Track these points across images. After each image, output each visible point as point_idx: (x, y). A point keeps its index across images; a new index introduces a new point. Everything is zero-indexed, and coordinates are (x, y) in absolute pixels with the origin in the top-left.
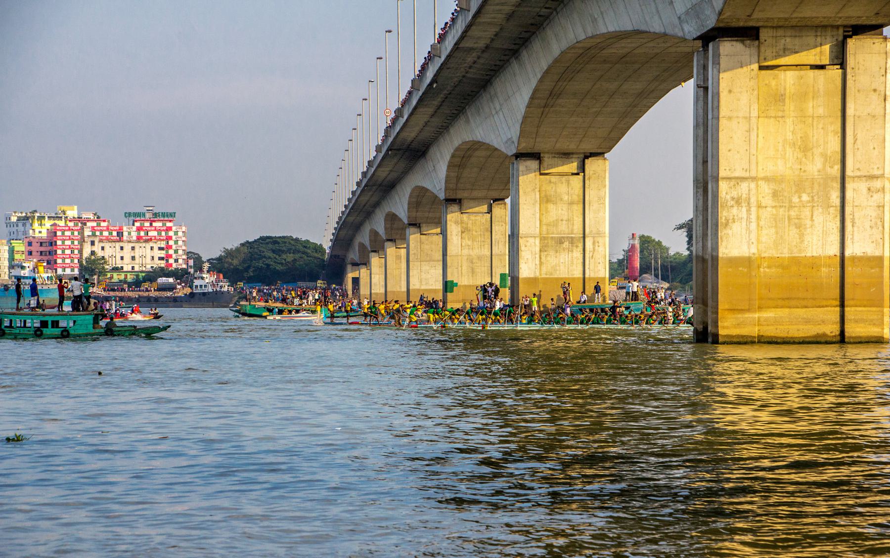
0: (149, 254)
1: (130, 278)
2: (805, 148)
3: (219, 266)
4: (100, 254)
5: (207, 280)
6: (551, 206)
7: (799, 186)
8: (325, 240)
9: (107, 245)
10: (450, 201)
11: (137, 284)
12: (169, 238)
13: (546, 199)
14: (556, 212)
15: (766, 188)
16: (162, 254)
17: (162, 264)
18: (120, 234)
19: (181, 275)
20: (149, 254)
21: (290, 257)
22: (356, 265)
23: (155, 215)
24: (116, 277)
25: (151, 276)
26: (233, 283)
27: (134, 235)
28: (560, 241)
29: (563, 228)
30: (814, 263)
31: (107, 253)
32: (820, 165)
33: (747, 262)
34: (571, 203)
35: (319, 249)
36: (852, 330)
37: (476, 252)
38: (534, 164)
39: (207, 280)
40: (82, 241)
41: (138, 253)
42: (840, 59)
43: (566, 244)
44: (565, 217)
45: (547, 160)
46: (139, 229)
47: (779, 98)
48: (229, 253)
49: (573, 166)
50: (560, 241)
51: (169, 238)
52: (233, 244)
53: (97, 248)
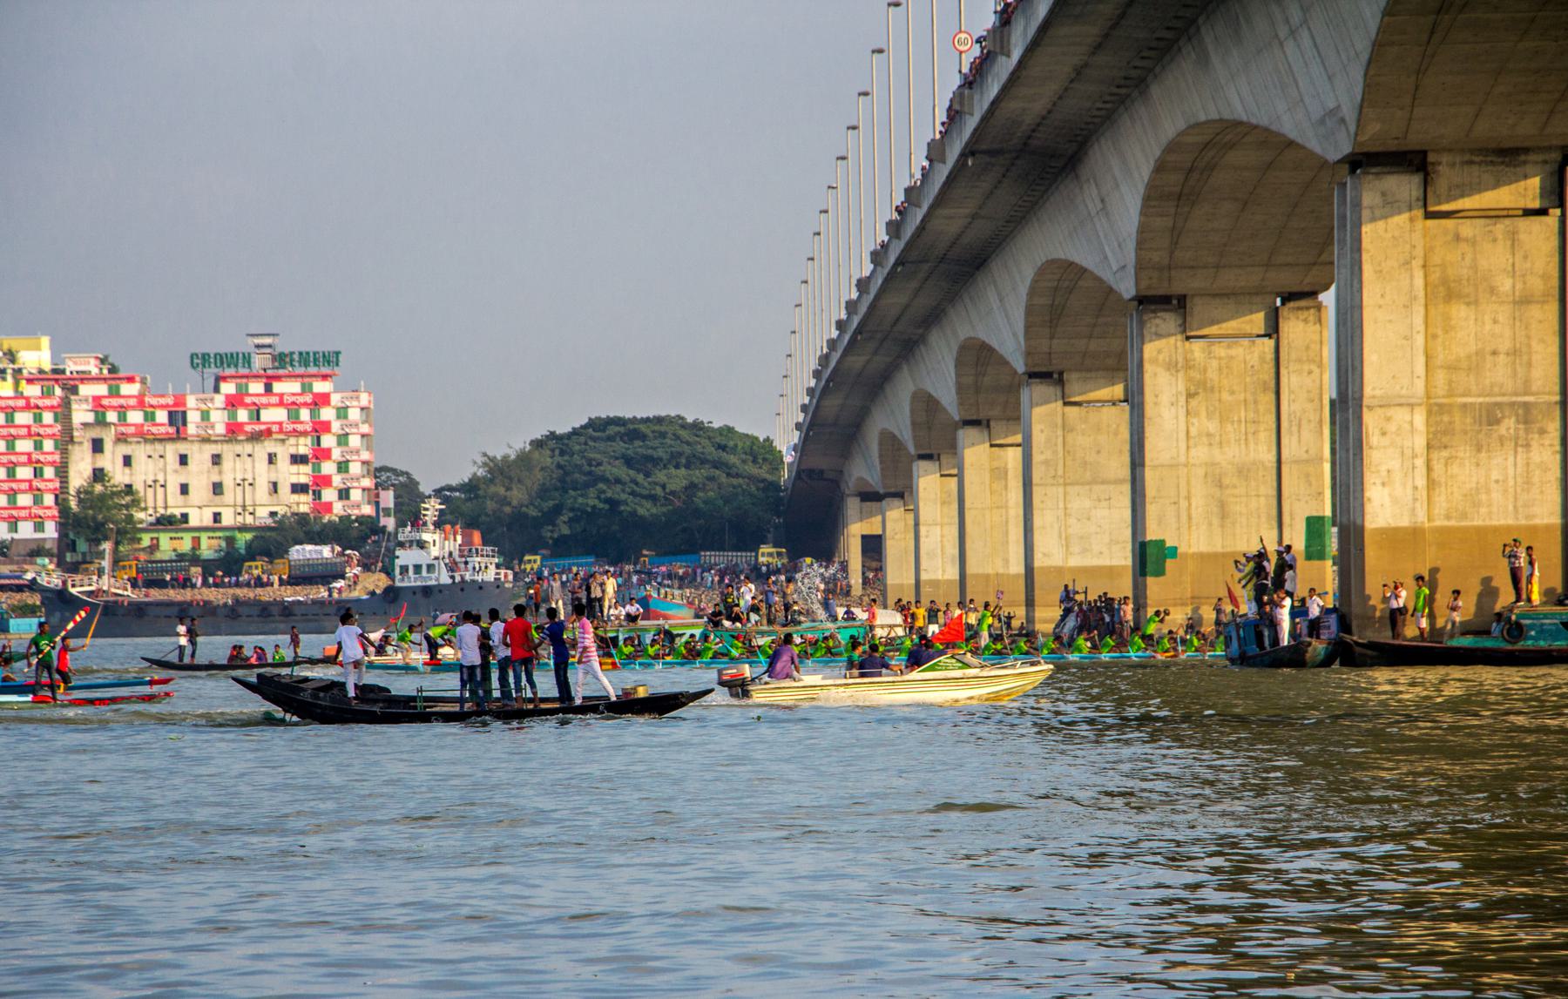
0: (263, 474)
1: (209, 547)
3: (469, 508)
4: (119, 476)
5: (434, 551)
6: (1459, 311)
9: (139, 452)
10: (1149, 302)
11: (229, 564)
12: (321, 428)
13: (1445, 291)
16: (303, 474)
17: (304, 504)
18: (177, 418)
19: (362, 538)
20: (263, 474)
21: (677, 479)
22: (871, 497)
23: (281, 359)
24: (169, 546)
25: (271, 541)
26: (510, 558)
27: (219, 419)
28: (1490, 416)
29: (1499, 374)
31: (143, 472)
34: (1524, 301)
35: (762, 451)
37: (1231, 454)
38: (1405, 185)
39: (434, 551)
40: (66, 439)
41: (230, 473)
43: (1509, 425)
45: (1446, 171)
46: (233, 403)
48: (500, 470)
49: (1258, 321)
50: (1490, 416)
51: (321, 428)
52: (511, 442)
53: (110, 460)
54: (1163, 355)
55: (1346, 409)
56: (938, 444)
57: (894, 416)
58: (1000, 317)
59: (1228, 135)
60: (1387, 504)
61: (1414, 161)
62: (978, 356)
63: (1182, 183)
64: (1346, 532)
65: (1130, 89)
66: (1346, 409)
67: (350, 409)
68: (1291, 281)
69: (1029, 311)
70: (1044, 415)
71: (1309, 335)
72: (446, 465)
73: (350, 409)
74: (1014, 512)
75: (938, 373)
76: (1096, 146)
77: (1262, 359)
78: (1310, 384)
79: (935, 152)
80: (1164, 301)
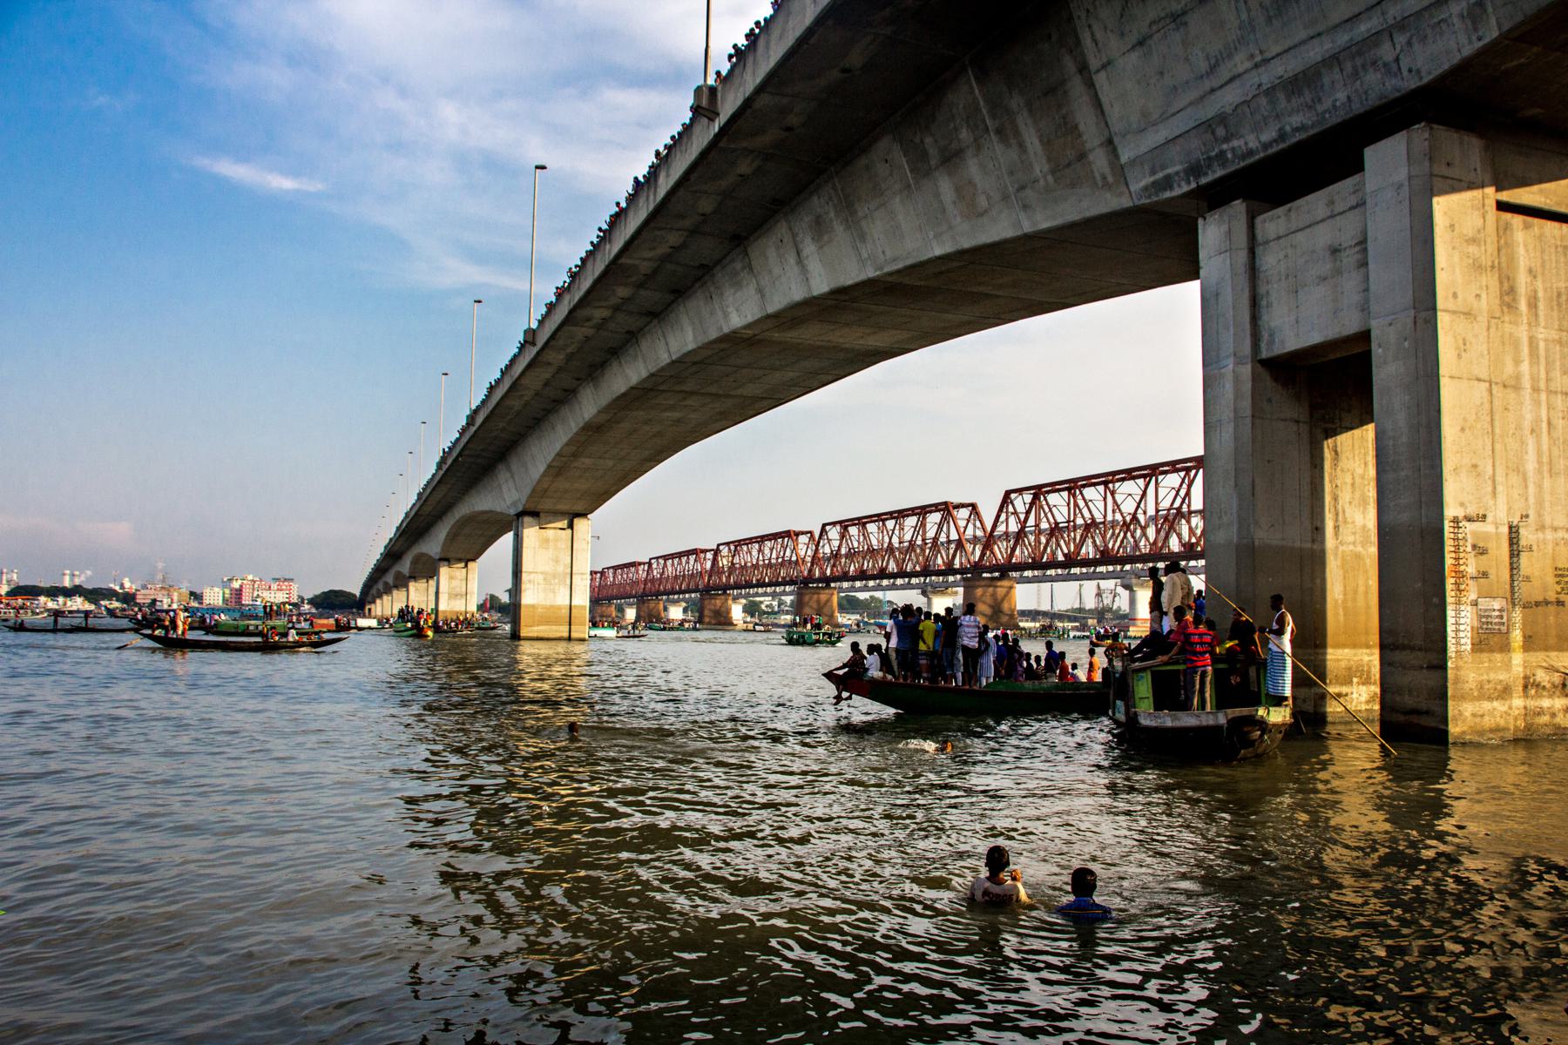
2: (557, 561)
3: (312, 602)
5: (306, 607)
7: (554, 576)
8: (356, 589)
13: (451, 578)
14: (455, 583)
15: (541, 577)
30: (559, 608)
32: (563, 568)
33: (533, 606)
36: (574, 635)
42: (571, 526)
44: (458, 585)
47: (547, 541)
49: (564, 524)
52: (318, 592)
54: (412, 585)
55: (437, 593)
56: (380, 596)
57: (374, 591)
58: (389, 578)
59: (423, 555)
60: (442, 607)
61: (535, 514)
62: (386, 583)
63: (415, 561)
64: (436, 610)
65: (409, 547)
66: (437, 593)
67: (295, 587)
68: (579, 508)
69: (549, 466)
70: (395, 592)
71: (432, 583)
72: (308, 595)
73: (295, 587)
74: (389, 606)
75: (380, 586)
76: (682, 308)
77: (1527, 227)
78: (432, 590)
79: (463, 432)
80: (414, 577)
